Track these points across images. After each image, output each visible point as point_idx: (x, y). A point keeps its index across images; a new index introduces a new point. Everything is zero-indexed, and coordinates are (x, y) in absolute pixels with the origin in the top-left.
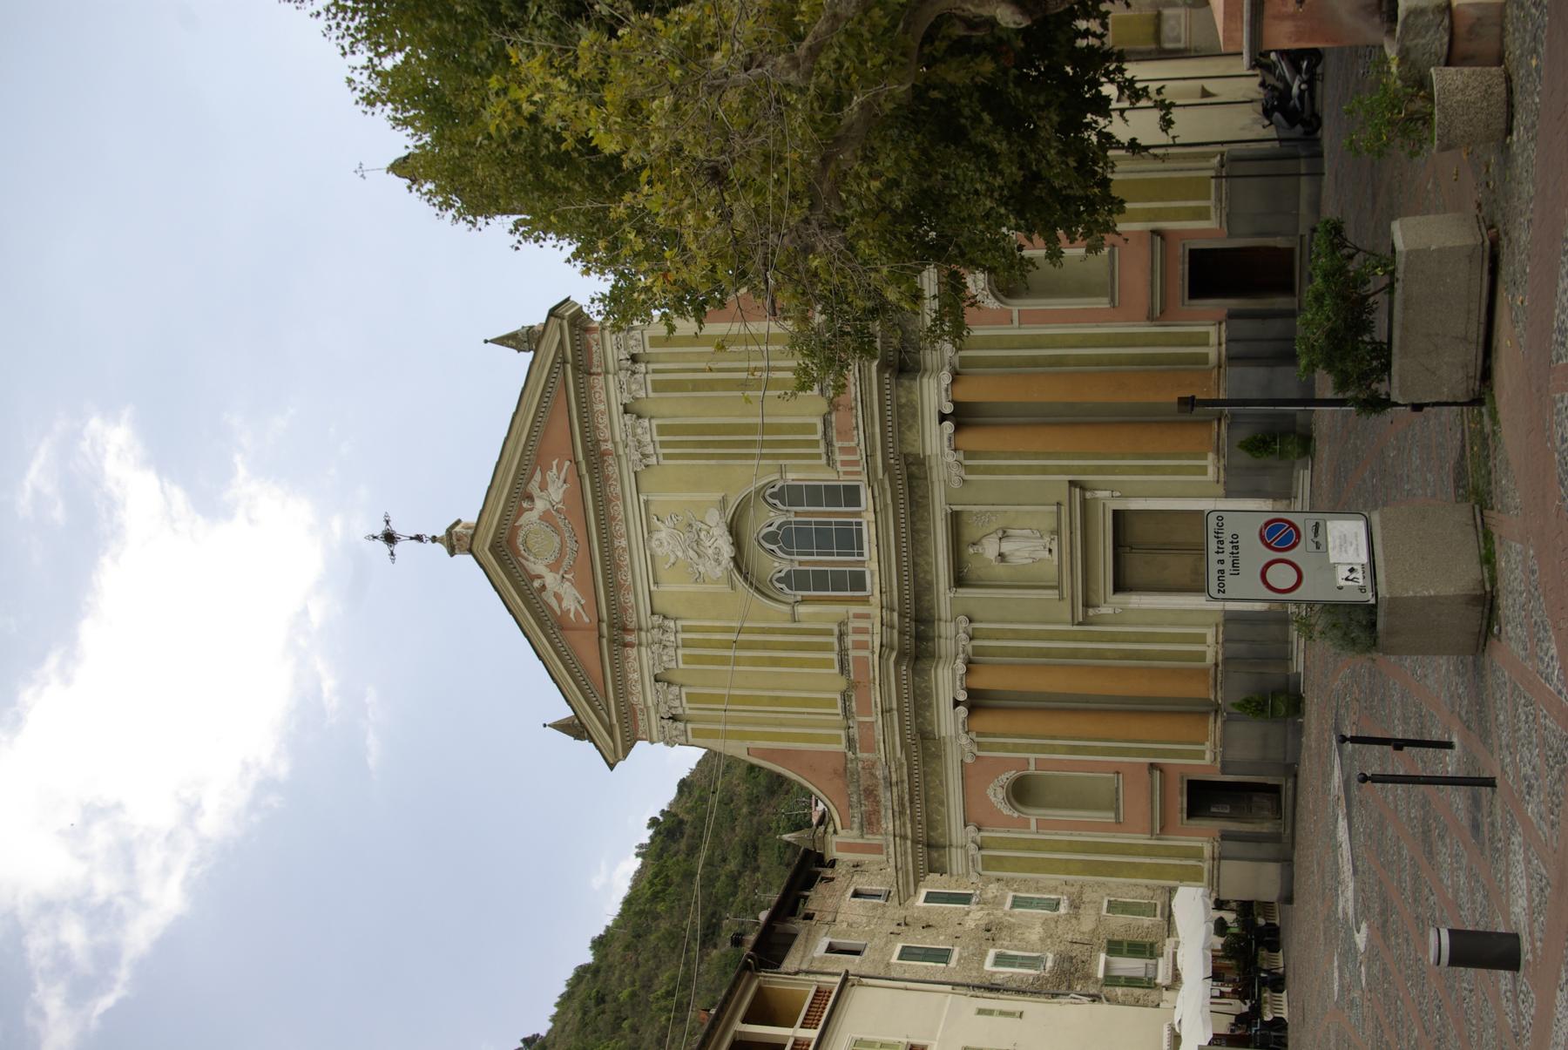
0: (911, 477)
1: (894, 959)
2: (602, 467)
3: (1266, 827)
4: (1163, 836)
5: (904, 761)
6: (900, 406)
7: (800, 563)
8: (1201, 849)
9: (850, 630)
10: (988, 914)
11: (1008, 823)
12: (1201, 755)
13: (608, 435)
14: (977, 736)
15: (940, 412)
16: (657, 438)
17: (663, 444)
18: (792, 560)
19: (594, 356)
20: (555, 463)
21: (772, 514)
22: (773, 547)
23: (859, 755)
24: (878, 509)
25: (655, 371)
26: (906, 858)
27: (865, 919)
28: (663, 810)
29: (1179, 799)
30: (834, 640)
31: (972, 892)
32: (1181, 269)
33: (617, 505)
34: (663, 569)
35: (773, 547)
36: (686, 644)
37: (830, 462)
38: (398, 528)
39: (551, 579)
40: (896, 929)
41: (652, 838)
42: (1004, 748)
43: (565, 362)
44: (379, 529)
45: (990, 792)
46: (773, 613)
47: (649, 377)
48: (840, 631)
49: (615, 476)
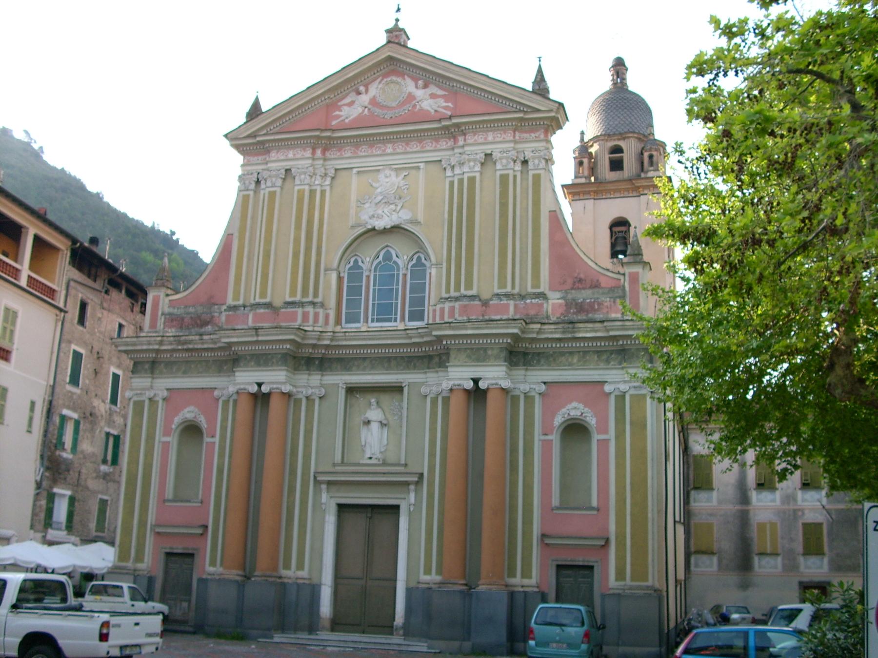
0: (430, 357)
1: (74, 347)
7: (368, 277)
11: (168, 421)
12: (213, 563)
16: (466, 176)
17: (461, 181)
18: (370, 270)
20: (450, 104)
21: (405, 257)
23: (224, 314)
25: (515, 177)
26: (146, 344)
27: (103, 329)
33: (417, 147)
36: (312, 192)
39: (365, 99)
42: (225, 419)
45: (191, 408)
46: (332, 255)
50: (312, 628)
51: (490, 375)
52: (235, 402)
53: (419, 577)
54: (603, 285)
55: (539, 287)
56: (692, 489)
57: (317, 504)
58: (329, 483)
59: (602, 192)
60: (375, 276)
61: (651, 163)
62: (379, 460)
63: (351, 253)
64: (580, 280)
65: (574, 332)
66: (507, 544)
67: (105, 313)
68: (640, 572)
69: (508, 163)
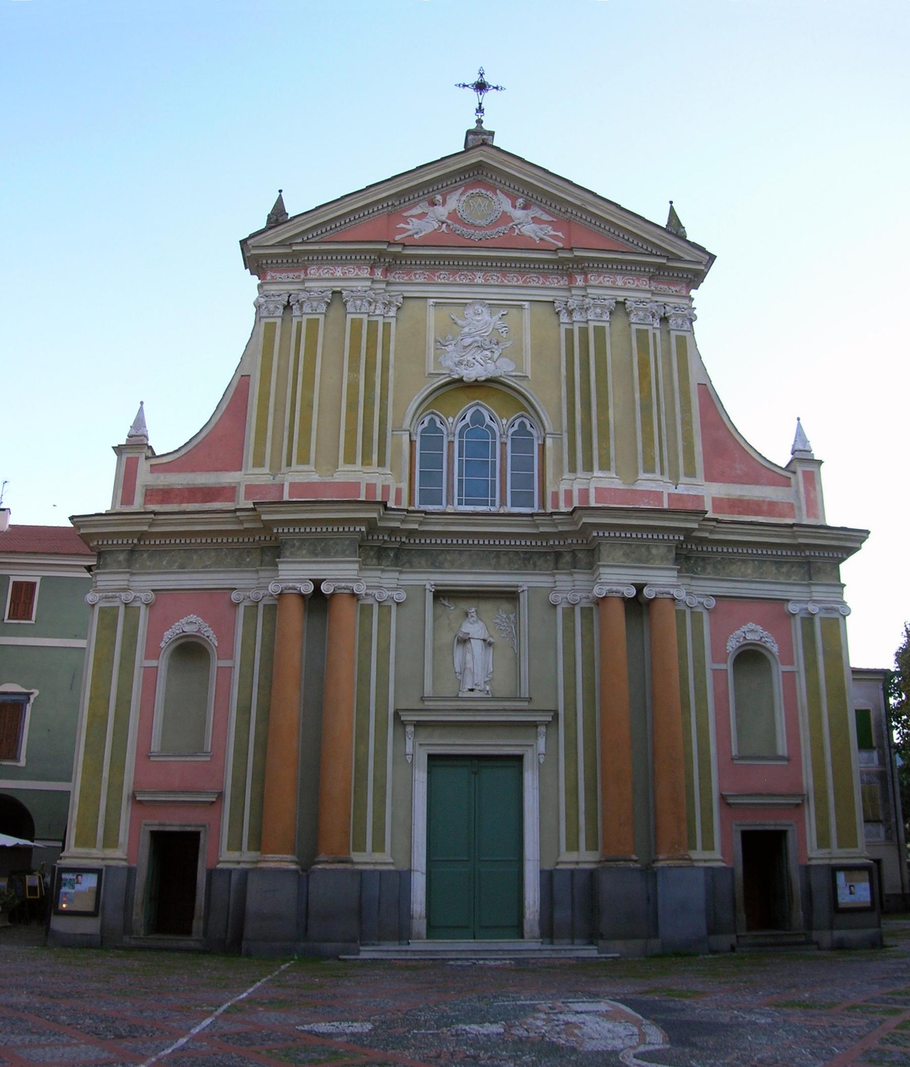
0: (558, 555)
2: (557, 274)
7: (451, 443)
11: (154, 636)
12: (236, 845)
15: (645, 585)
16: (592, 325)
17: (584, 332)
20: (560, 234)
22: (468, 418)
29: (156, 822)
32: (770, 824)
33: (518, 280)
34: (454, 313)
35: (468, 418)
36: (372, 325)
38: (490, 95)
39: (442, 212)
43: (668, 259)
47: (650, 328)
58: (418, 725)
60: (461, 443)
69: (646, 316)
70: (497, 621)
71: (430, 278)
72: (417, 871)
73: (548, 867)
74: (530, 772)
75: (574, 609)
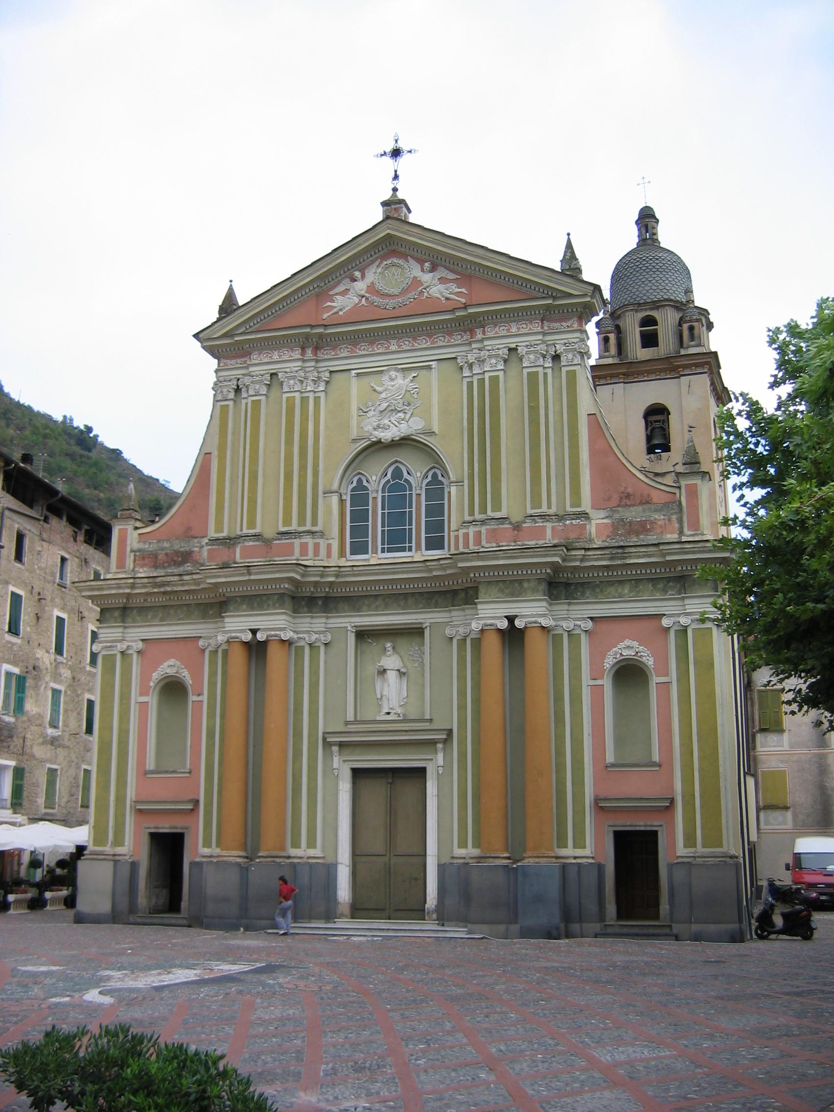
0: (455, 593)
1: (12, 588)
3: (142, 900)
4: (133, 811)
5: (202, 586)
6: (520, 582)
7: (375, 498)
8: (122, 844)
9: (317, 541)
10: (47, 669)
11: (145, 677)
12: (207, 843)
13: (489, 335)
14: (224, 650)
17: (481, 382)
18: (378, 491)
19: (559, 324)
20: (463, 290)
21: (419, 474)
23: (206, 548)
24: (428, 564)
25: (545, 374)
27: (43, 565)
28: (98, 436)
29: (152, 826)
30: (308, 527)
31: (65, 656)
32: (640, 824)
33: (427, 342)
34: (372, 381)
36: (305, 400)
37: (466, 524)
38: (404, 159)
39: (361, 286)
40: (36, 590)
41: (77, 428)
42: (213, 674)
44: (403, 145)
45: (172, 662)
47: (540, 369)
48: (316, 532)
49: (452, 340)
50: (330, 915)
51: (525, 612)
52: (226, 653)
53: (453, 851)
54: (655, 499)
55: (580, 506)
56: (757, 732)
57: (329, 771)
58: (342, 745)
59: (632, 374)
61: (692, 337)
62: (399, 715)
63: (353, 472)
64: (628, 496)
65: (625, 558)
66: (555, 810)
67: (45, 544)
68: (714, 836)
69: (537, 359)
70: (411, 653)
71: (352, 351)
72: (341, 864)
73: (443, 861)
74: (431, 781)
75: (465, 640)
